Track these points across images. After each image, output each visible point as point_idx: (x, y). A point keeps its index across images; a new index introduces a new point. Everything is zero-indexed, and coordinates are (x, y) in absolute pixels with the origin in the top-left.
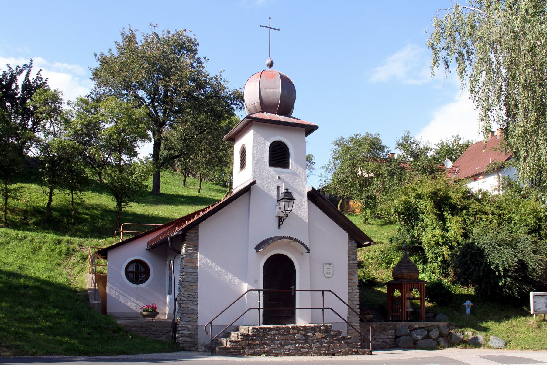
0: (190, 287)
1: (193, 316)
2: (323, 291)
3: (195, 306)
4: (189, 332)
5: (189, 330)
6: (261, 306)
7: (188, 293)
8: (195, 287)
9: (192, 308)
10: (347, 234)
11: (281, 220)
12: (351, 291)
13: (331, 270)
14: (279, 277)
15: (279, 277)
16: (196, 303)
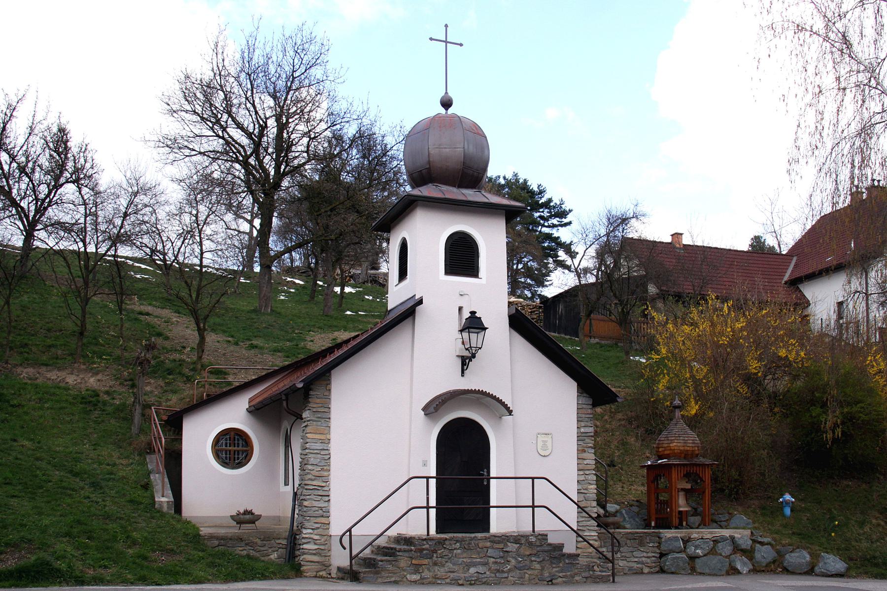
0: (317, 474)
1: (323, 520)
2: (533, 479)
3: (326, 504)
4: (316, 547)
5: (315, 544)
6: (433, 502)
7: (314, 483)
8: (326, 474)
9: (321, 508)
10: (576, 384)
11: (465, 362)
12: (582, 478)
13: (549, 444)
14: (463, 454)
15: (463, 454)
16: (326, 499)
